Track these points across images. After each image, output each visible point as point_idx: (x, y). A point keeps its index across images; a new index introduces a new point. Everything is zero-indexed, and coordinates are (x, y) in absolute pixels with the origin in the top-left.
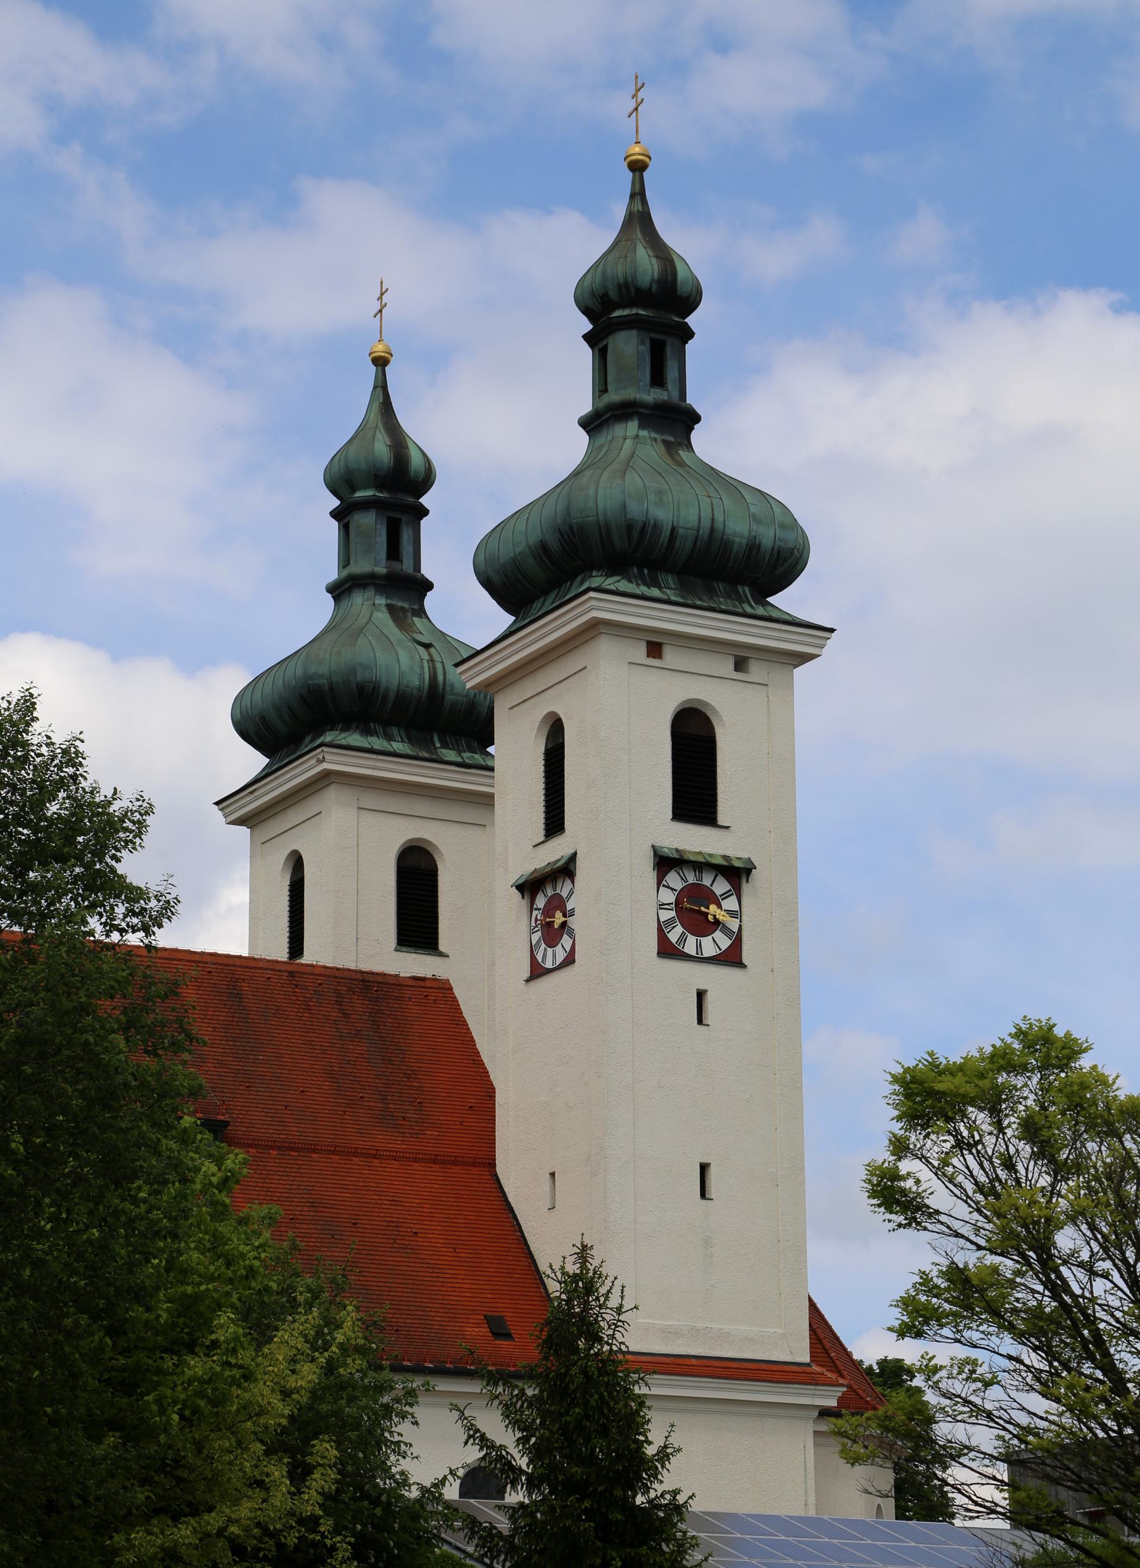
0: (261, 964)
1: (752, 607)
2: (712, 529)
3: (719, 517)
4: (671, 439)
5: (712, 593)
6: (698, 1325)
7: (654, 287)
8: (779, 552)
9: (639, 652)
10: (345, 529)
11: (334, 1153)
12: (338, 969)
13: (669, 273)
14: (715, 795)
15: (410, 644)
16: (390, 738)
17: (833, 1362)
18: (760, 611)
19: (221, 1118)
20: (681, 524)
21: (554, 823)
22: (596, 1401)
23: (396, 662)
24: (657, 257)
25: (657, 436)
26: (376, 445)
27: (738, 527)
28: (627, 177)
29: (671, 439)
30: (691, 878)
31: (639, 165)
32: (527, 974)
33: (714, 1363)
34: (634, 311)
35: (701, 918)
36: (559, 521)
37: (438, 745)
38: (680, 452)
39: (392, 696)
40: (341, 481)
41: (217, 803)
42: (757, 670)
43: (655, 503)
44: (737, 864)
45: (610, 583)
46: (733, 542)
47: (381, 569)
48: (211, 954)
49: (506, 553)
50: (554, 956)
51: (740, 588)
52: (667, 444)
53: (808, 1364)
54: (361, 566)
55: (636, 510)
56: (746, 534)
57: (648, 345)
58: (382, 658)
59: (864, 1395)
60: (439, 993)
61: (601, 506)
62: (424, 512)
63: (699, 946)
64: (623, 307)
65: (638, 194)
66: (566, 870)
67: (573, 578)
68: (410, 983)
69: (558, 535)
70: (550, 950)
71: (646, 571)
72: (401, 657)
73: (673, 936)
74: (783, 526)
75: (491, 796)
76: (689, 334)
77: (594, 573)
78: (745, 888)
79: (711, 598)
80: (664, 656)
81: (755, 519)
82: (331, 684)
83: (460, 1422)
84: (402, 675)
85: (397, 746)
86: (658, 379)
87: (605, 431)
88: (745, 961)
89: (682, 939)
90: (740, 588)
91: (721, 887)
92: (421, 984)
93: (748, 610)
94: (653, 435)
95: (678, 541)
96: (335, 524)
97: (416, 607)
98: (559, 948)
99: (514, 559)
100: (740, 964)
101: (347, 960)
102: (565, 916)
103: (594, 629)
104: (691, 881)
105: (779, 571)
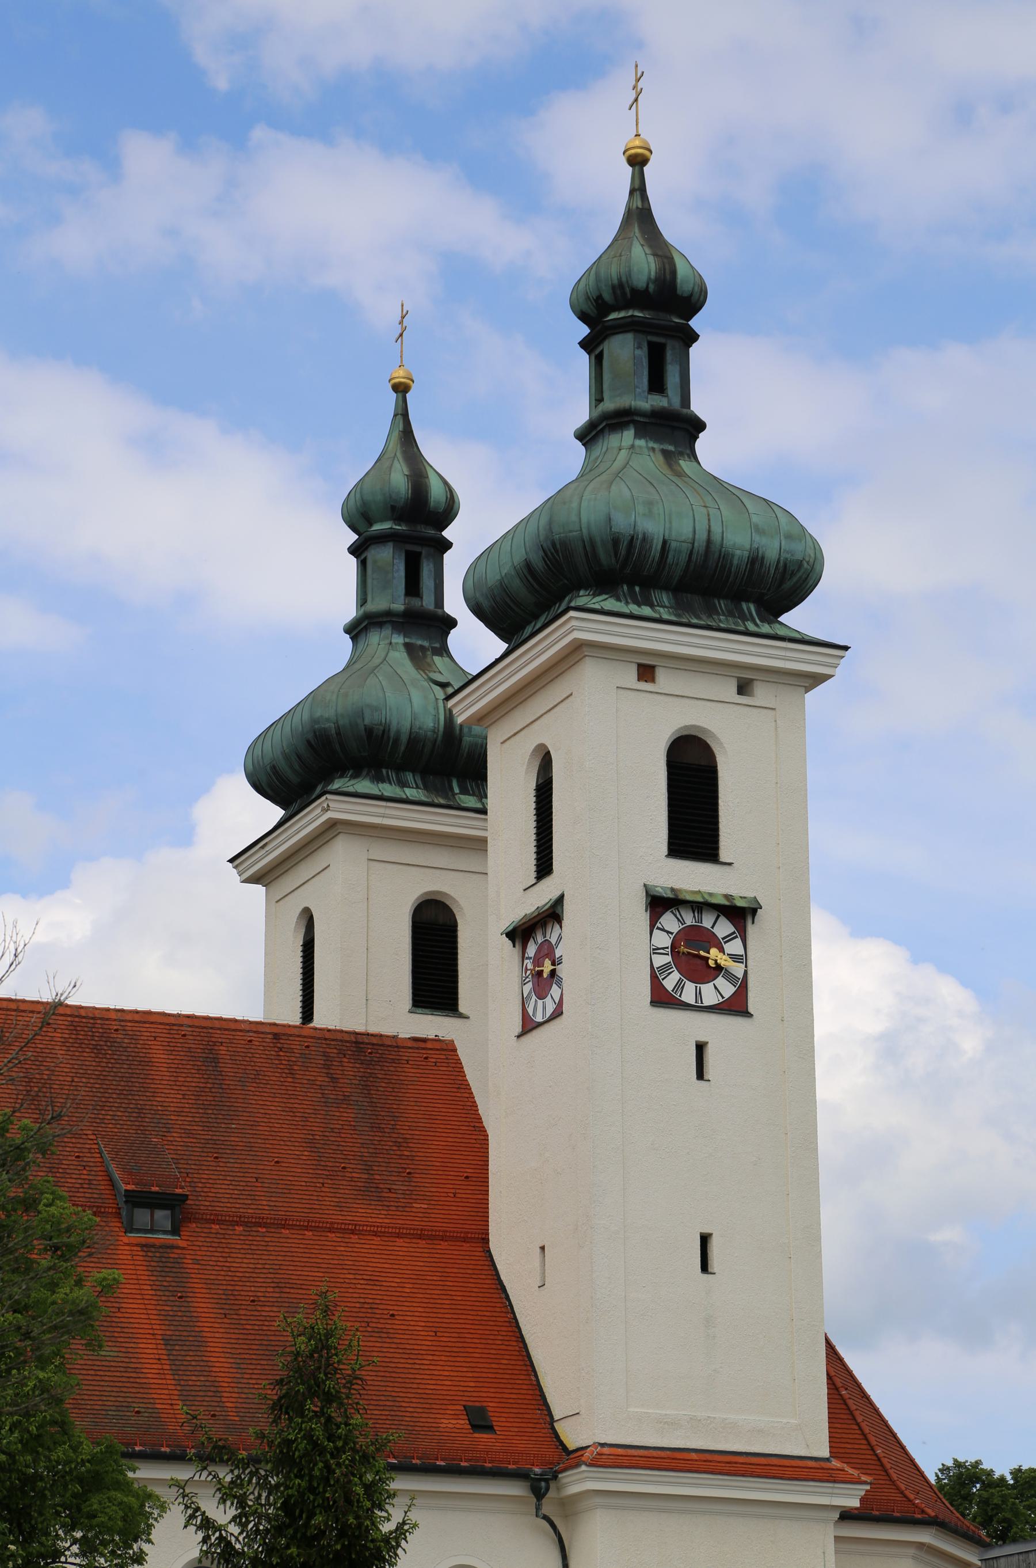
0: (243, 1026)
1: (757, 625)
2: (709, 541)
3: (716, 529)
4: (671, 448)
5: (711, 611)
7: (652, 287)
8: (785, 565)
9: (629, 676)
10: (363, 565)
11: (307, 1228)
12: (329, 1030)
13: (667, 271)
14: (717, 830)
15: (425, 684)
16: (403, 784)
17: (879, 1460)
18: (765, 629)
19: (178, 1191)
21: (544, 867)
22: (320, 1470)
23: (408, 700)
24: (655, 255)
25: (656, 446)
26: (392, 475)
27: (738, 540)
29: (671, 448)
30: (689, 919)
31: (639, 159)
32: (518, 1029)
33: (741, 1459)
34: (630, 313)
35: (699, 962)
36: (542, 538)
37: (457, 790)
38: (681, 462)
39: (404, 739)
40: (360, 515)
41: (231, 861)
42: (762, 694)
43: (644, 515)
44: (740, 903)
45: (597, 602)
46: (733, 555)
47: (399, 606)
48: (188, 1016)
49: (493, 577)
50: (544, 1008)
51: (744, 605)
52: (665, 453)
53: (827, 1460)
54: (378, 604)
55: (622, 523)
56: (748, 547)
57: (645, 349)
58: (392, 698)
59: (912, 1497)
60: (443, 1056)
61: (584, 520)
62: (447, 545)
63: (699, 994)
64: (618, 309)
65: (639, 189)
66: (552, 914)
67: (561, 599)
68: (410, 1044)
69: (541, 553)
70: (540, 1002)
71: (637, 589)
72: (412, 695)
73: (669, 983)
74: (789, 537)
75: (484, 841)
76: (692, 337)
77: (582, 593)
78: (751, 929)
79: (710, 616)
80: (657, 679)
81: (758, 530)
82: (338, 729)
83: (180, 1500)
84: (414, 716)
85: (410, 793)
86: (657, 384)
87: (601, 441)
88: (751, 1010)
89: (679, 986)
90: (744, 605)
91: (723, 928)
92: (422, 1045)
93: (752, 627)
94: (651, 444)
95: (670, 556)
96: (353, 561)
97: (437, 645)
98: (548, 999)
99: (501, 582)
100: (746, 1013)
101: (356, 1023)
102: (553, 964)
103: (578, 651)
104: (689, 923)
105: (788, 585)
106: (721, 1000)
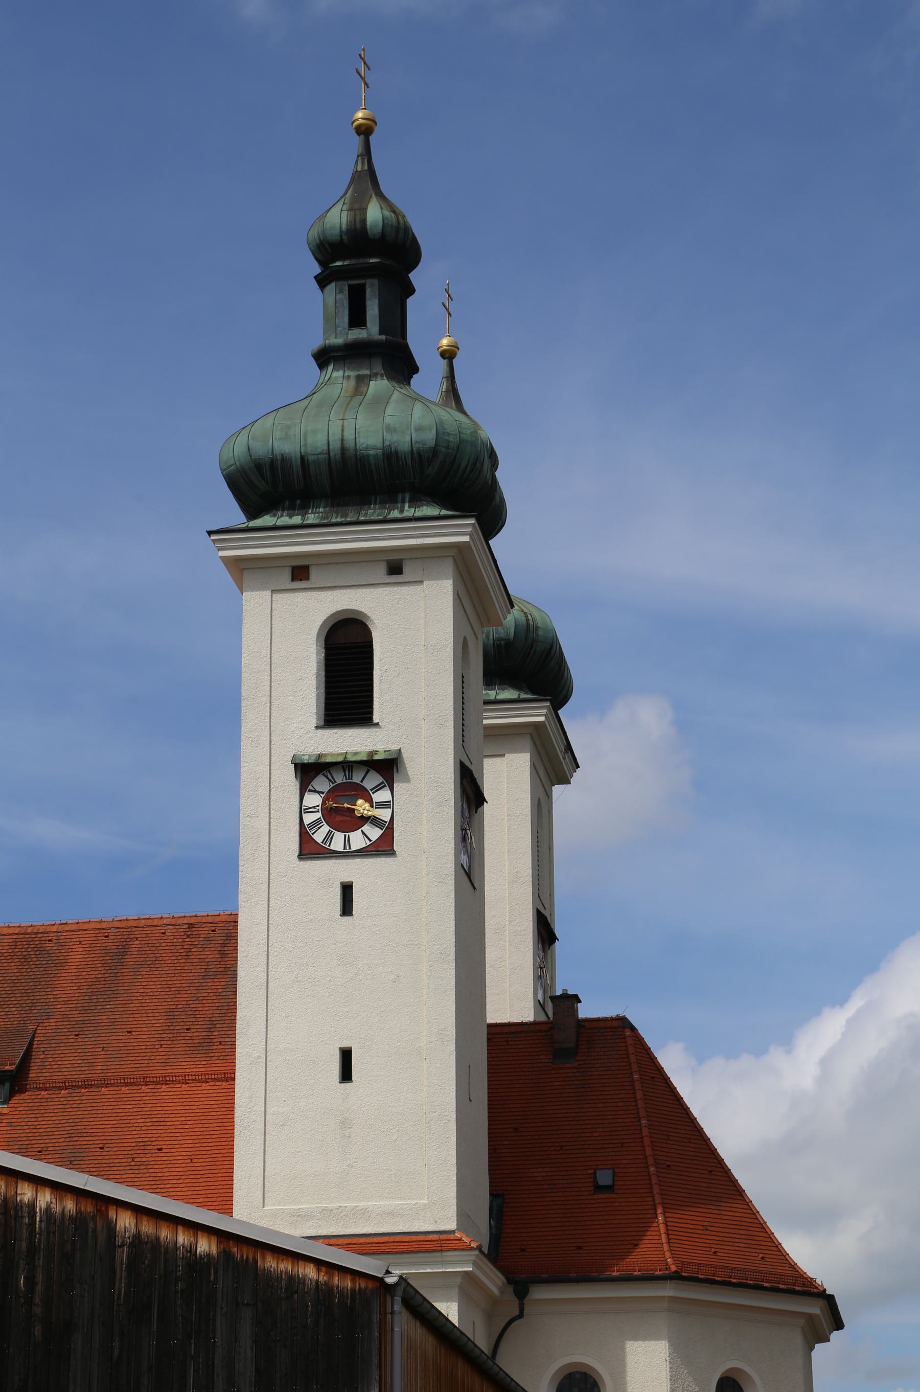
6: (331, 1206)
7: (345, 237)
20: (309, 450)
28: (357, 142)
30: (340, 778)
43: (280, 439)
55: (261, 449)
56: (380, 445)
57: (346, 292)
63: (347, 841)
65: (451, 376)
73: (319, 837)
89: (329, 837)
91: (372, 780)
106: (369, 843)
